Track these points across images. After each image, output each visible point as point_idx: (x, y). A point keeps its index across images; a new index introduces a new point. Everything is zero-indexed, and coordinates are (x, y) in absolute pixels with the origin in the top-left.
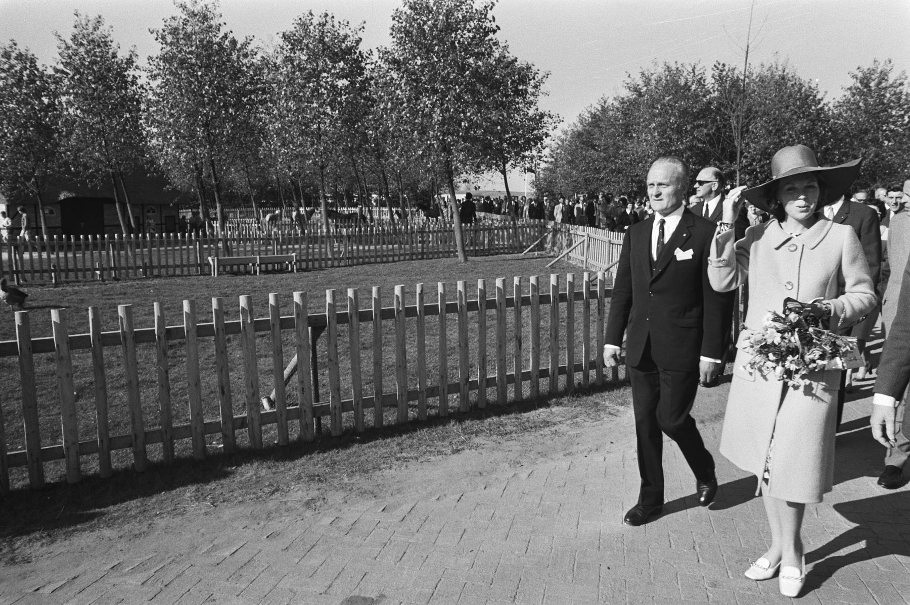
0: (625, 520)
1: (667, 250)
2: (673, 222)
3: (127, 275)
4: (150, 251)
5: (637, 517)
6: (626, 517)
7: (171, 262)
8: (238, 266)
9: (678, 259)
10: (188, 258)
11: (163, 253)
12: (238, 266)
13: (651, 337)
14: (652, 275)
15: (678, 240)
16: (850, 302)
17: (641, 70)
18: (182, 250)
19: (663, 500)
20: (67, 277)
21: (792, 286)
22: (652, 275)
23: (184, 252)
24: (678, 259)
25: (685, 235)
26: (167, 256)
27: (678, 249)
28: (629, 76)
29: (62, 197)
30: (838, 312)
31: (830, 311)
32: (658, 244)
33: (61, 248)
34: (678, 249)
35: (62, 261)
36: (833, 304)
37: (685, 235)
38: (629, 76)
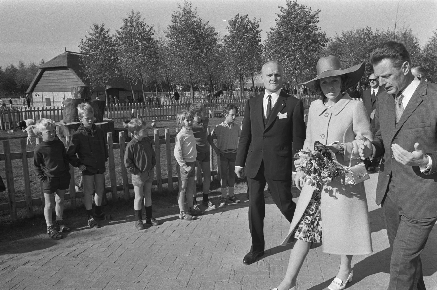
0: (243, 262)
1: (273, 112)
2: (275, 97)
3: (118, 121)
4: (139, 111)
5: (249, 260)
6: (244, 260)
7: (162, 114)
8: (217, 114)
9: (280, 118)
10: (160, 113)
11: (154, 111)
12: (217, 114)
13: (264, 162)
14: (265, 128)
15: (279, 107)
16: (346, 148)
17: (342, 31)
18: (158, 110)
19: (264, 249)
20: (160, 118)
21: (324, 136)
22: (265, 128)
23: (159, 111)
24: (280, 118)
25: (282, 105)
26: (161, 111)
27: (279, 112)
28: (336, 34)
29: (107, 88)
30: (349, 150)
31: (343, 150)
32: (267, 109)
33: (122, 109)
34: (279, 112)
35: (113, 115)
36: (346, 145)
37: (282, 105)
38: (336, 34)
